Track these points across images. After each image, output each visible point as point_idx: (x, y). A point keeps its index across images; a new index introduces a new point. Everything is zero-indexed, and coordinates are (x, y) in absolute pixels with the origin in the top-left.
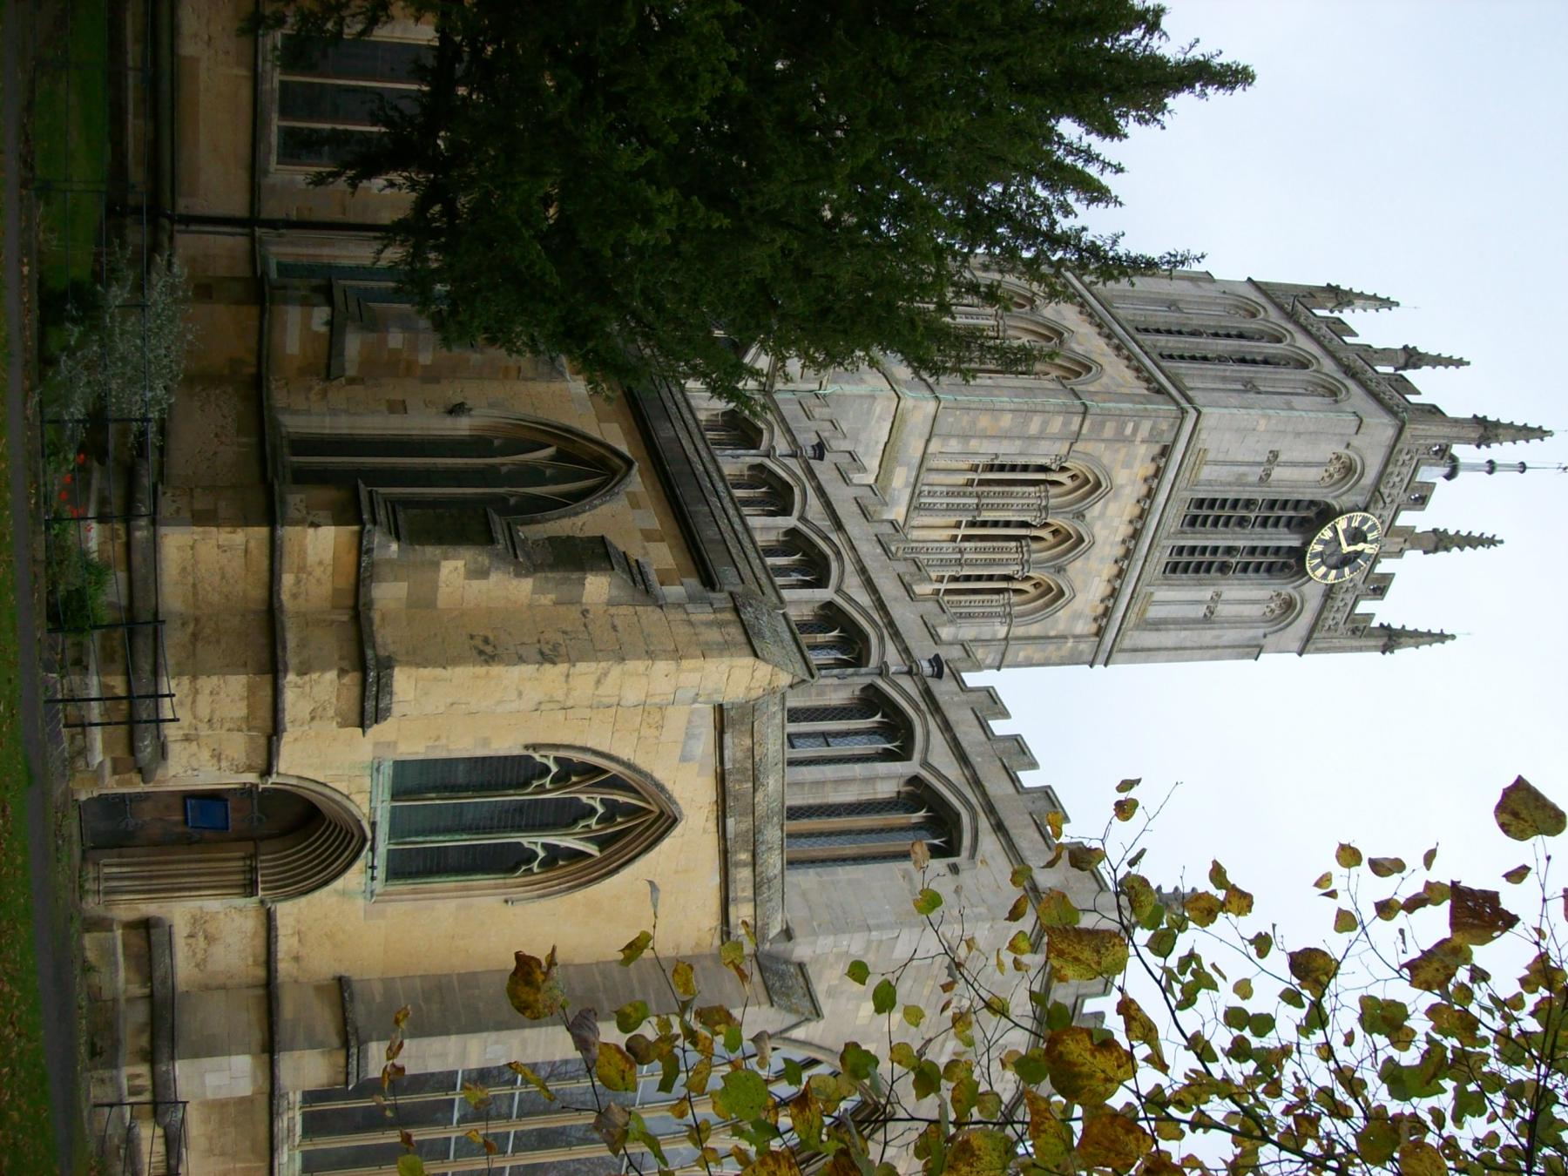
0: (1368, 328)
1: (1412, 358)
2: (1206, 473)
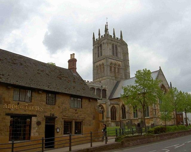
0: (97, 37)
1: (99, 34)
2: (111, 54)
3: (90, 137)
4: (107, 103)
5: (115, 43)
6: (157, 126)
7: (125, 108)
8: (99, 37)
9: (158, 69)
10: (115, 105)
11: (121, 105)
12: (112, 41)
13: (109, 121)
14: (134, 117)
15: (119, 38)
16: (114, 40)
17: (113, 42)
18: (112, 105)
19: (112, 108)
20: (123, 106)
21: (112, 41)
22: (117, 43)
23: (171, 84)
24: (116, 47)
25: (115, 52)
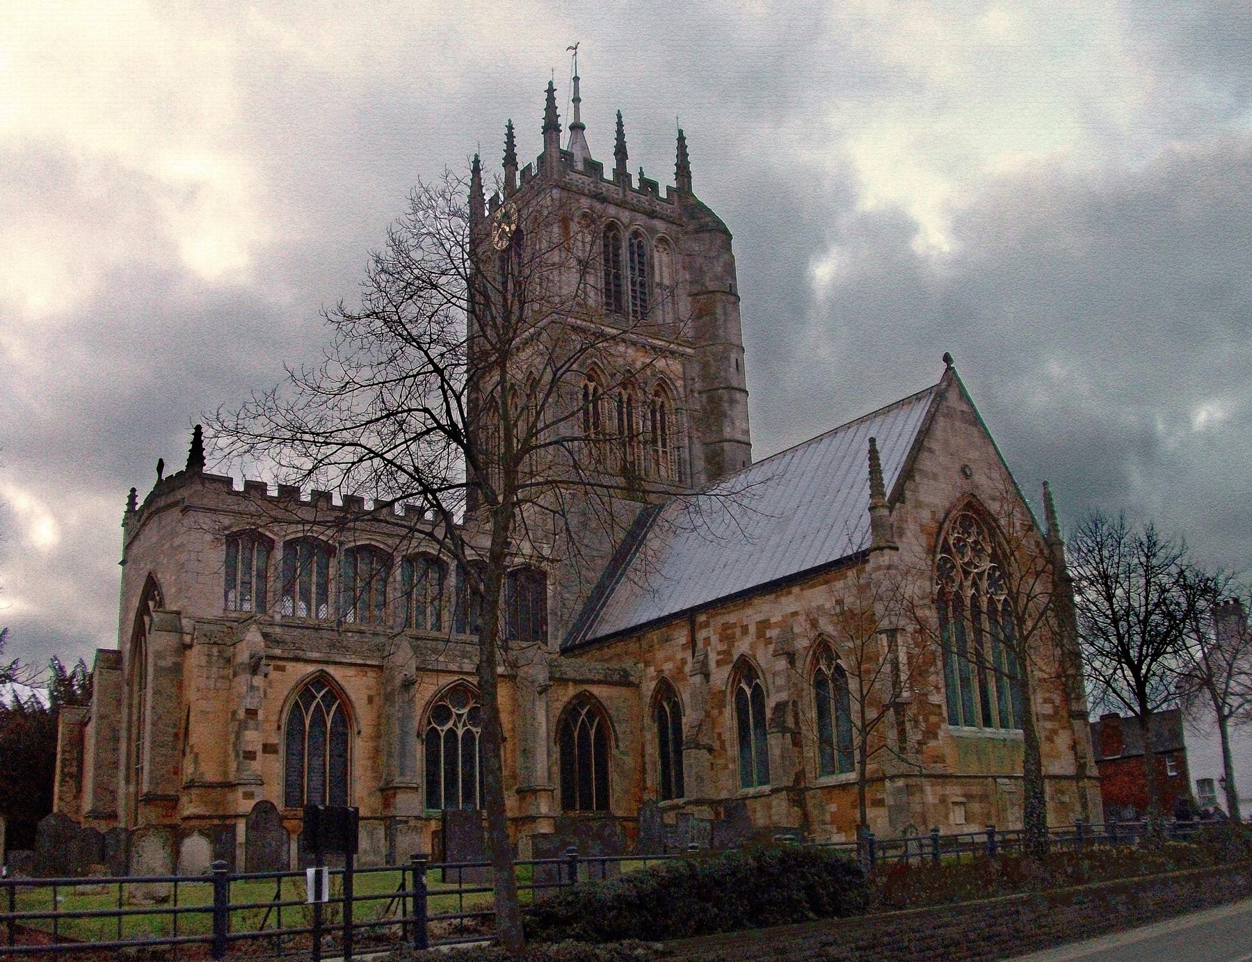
1: (510, 160)
3: (208, 919)
4: (521, 673)
5: (625, 216)
6: (281, 711)
7: (677, 712)
8: (509, 180)
9: (935, 376)
10: (596, 690)
11: (649, 687)
12: (603, 199)
13: (533, 819)
14: (747, 783)
15: (666, 179)
16: (615, 193)
17: (612, 210)
18: (571, 691)
19: (571, 711)
20: (666, 689)
21: (603, 199)
22: (641, 219)
23: (1047, 498)
24: (638, 252)
25: (626, 291)
